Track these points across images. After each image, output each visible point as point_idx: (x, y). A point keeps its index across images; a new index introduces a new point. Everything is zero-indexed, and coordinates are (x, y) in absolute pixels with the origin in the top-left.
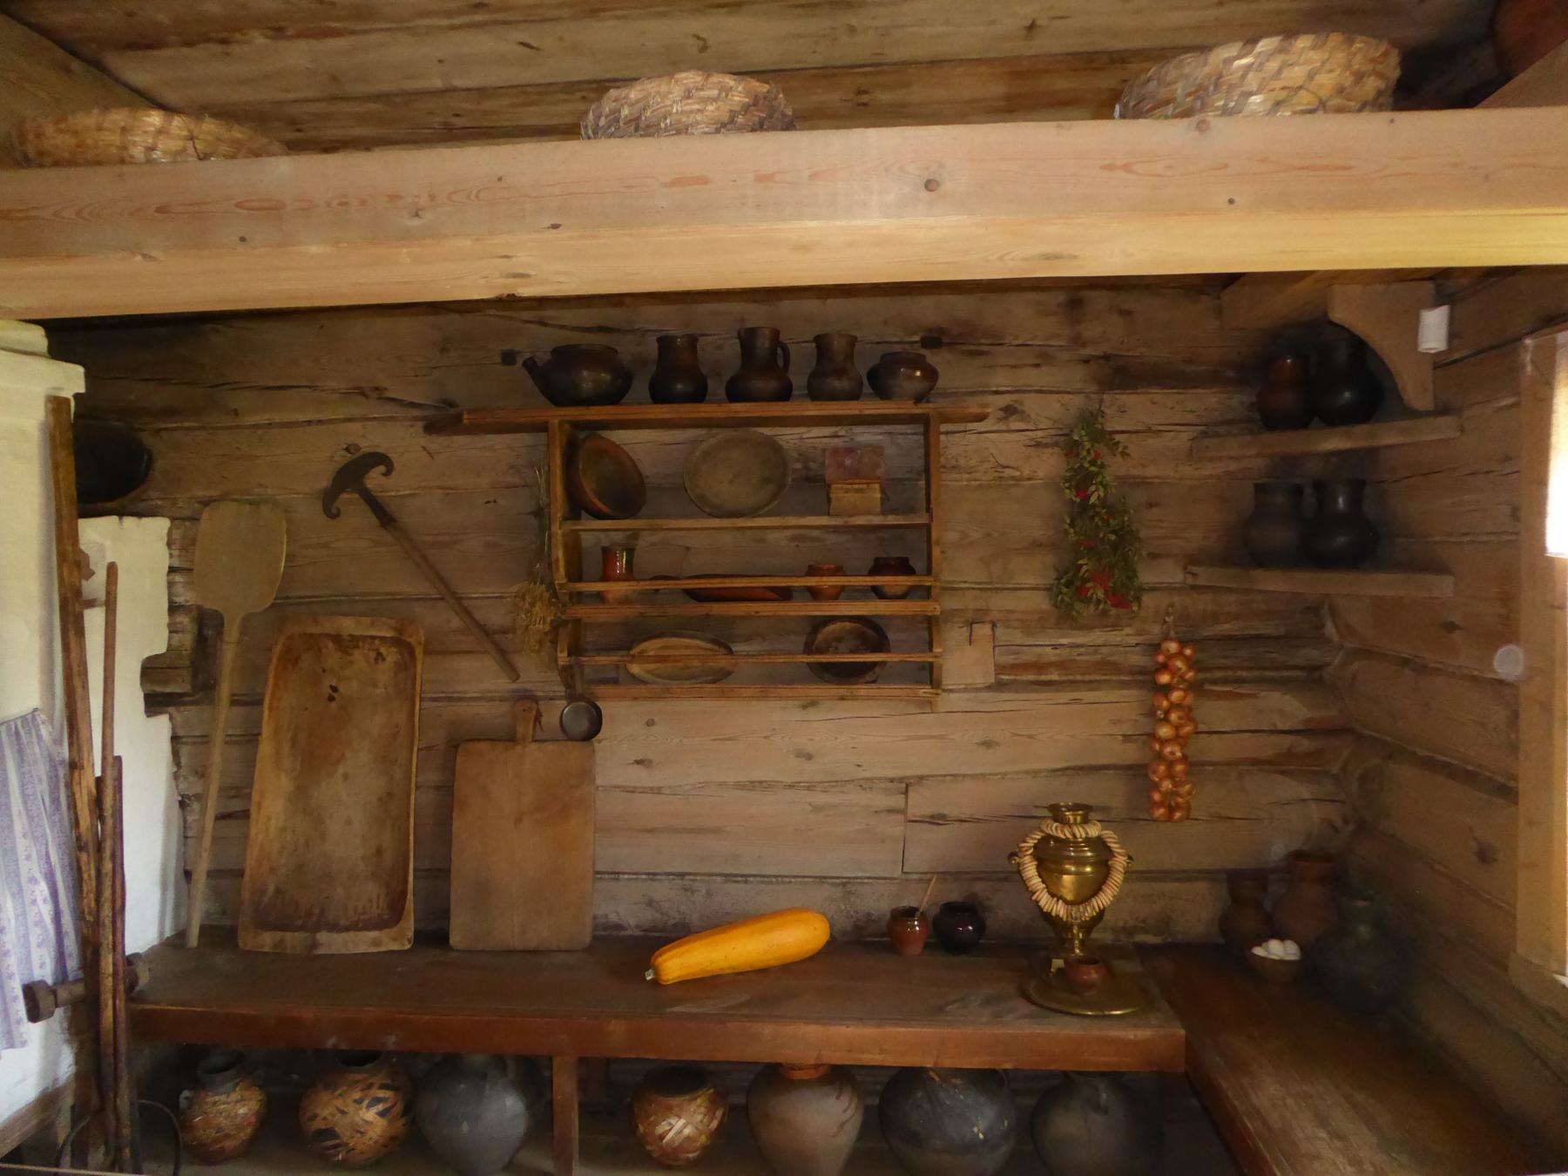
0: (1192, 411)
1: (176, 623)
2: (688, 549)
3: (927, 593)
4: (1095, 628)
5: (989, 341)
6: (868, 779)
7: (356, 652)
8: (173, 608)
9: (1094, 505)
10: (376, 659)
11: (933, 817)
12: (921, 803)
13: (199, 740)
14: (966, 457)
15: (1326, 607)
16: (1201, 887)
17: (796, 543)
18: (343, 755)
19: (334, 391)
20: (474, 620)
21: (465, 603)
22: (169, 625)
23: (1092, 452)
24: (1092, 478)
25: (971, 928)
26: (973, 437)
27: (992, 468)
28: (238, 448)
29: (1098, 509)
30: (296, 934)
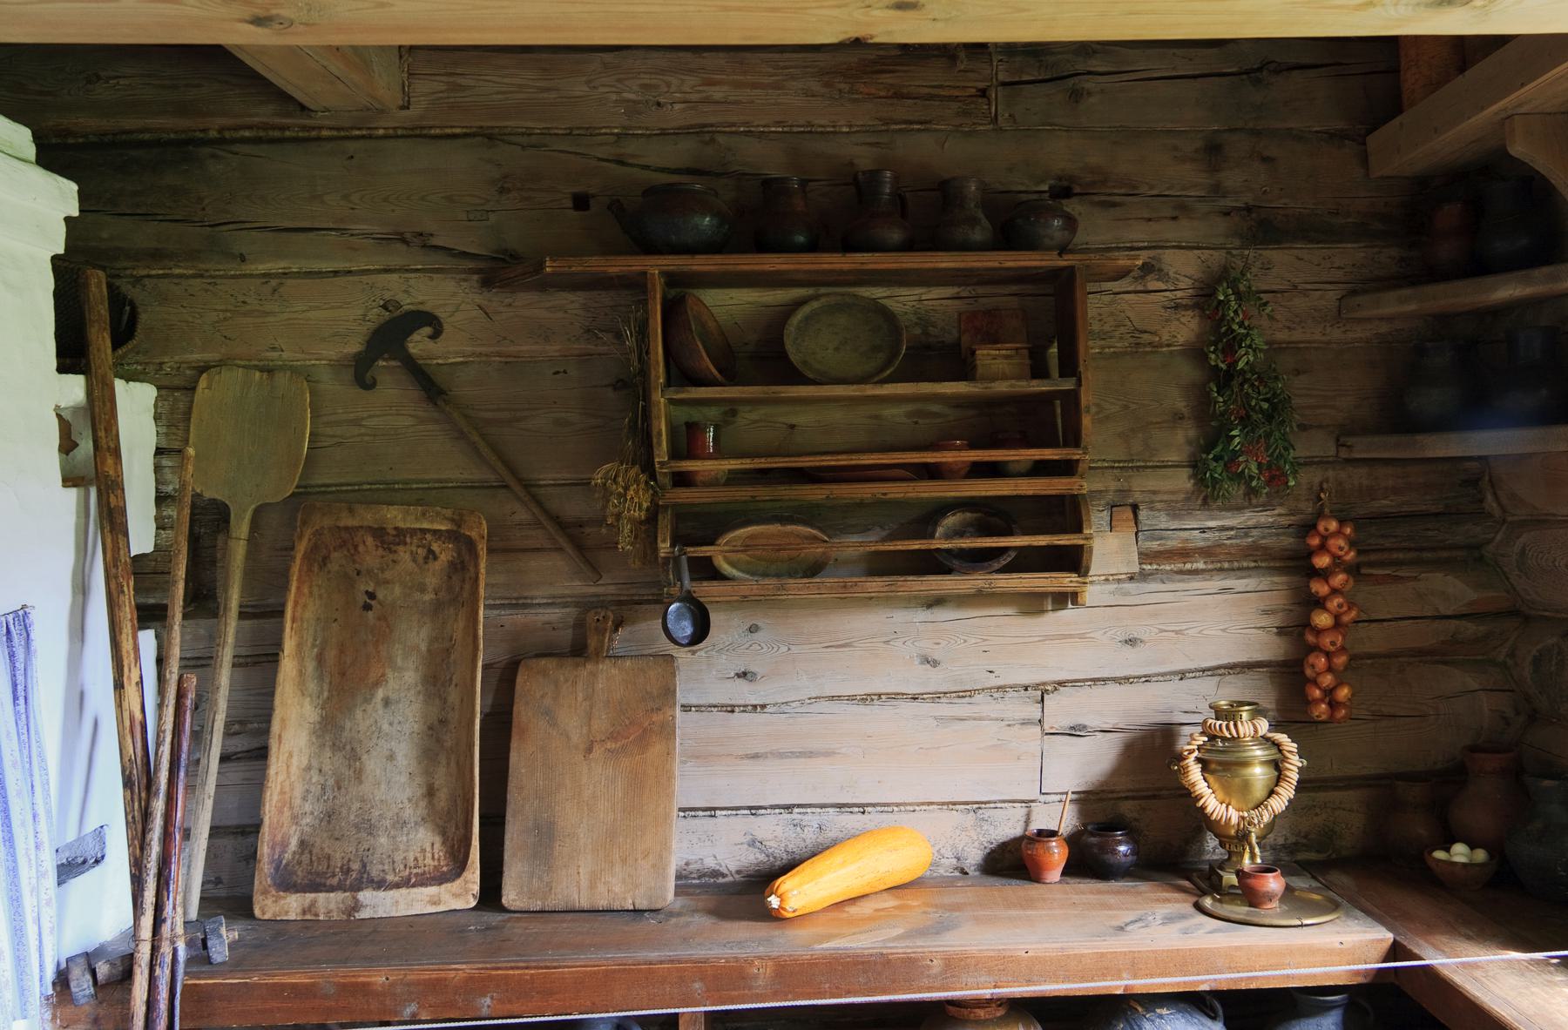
0: (1339, 268)
1: (165, 517)
2: (793, 427)
3: (1067, 468)
4: (1244, 508)
5: (1123, 191)
6: (998, 688)
7: (401, 548)
9: (1242, 371)
10: (426, 559)
11: (1072, 728)
13: (192, 663)
14: (1100, 320)
15: (1487, 478)
16: (1350, 797)
18: (383, 675)
19: (366, 235)
20: (546, 511)
21: (533, 490)
22: (156, 519)
23: (1240, 312)
24: (1242, 340)
26: (1107, 299)
28: (244, 302)
29: (1248, 376)
30: (332, 895)
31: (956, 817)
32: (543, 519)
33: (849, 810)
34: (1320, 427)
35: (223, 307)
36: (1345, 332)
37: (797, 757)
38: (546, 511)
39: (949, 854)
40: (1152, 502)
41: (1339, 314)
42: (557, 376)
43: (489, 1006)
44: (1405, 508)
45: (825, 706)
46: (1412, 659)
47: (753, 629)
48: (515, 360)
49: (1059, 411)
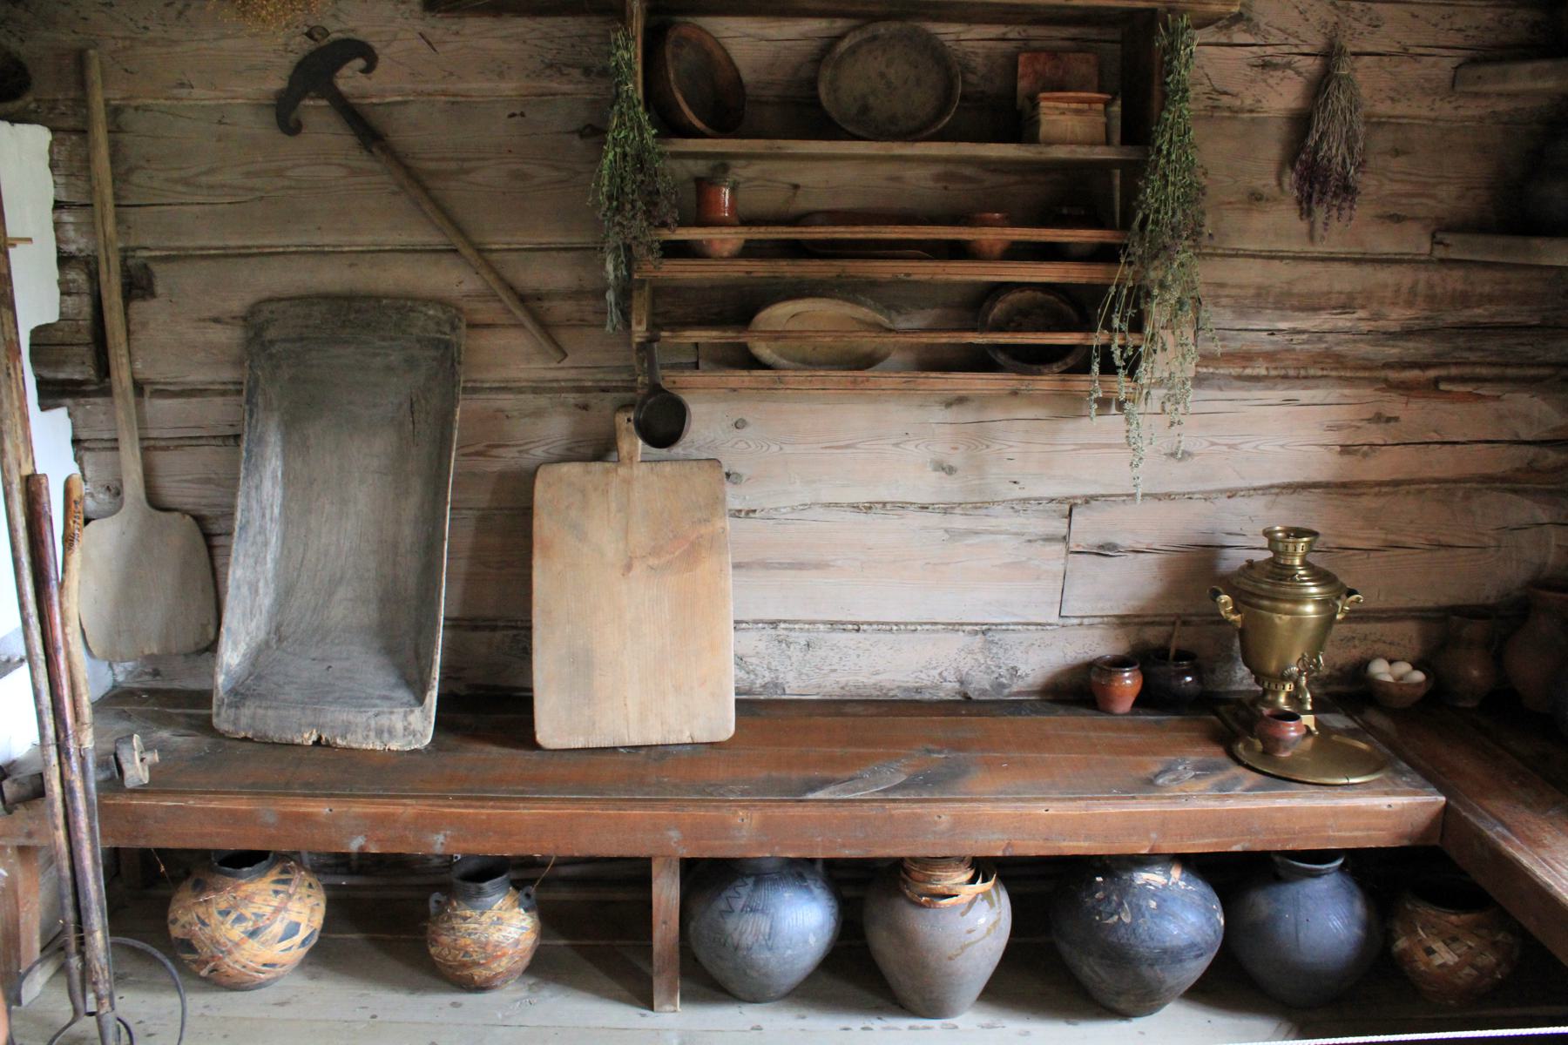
0: (1459, 30)
2: (796, 187)
8: (64, 260)
11: (1101, 547)
12: (1087, 526)
17: (944, 184)
20: (501, 279)
22: (60, 283)
25: (1189, 679)
27: (1204, 93)
31: (960, 639)
32: (496, 287)
33: (842, 627)
34: (1414, 219)
35: (121, 34)
36: (1456, 108)
37: (786, 568)
38: (501, 279)
39: (952, 678)
40: (1219, 296)
41: (1453, 86)
42: (514, 120)
43: (442, 844)
44: (1498, 319)
45: (818, 512)
46: (1480, 486)
47: (739, 425)
48: (463, 99)
49: (1117, 182)
